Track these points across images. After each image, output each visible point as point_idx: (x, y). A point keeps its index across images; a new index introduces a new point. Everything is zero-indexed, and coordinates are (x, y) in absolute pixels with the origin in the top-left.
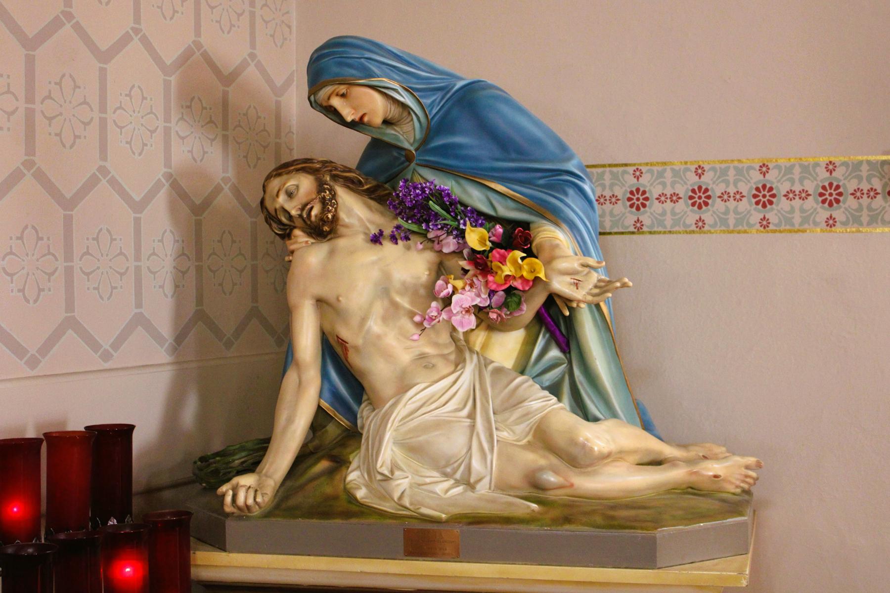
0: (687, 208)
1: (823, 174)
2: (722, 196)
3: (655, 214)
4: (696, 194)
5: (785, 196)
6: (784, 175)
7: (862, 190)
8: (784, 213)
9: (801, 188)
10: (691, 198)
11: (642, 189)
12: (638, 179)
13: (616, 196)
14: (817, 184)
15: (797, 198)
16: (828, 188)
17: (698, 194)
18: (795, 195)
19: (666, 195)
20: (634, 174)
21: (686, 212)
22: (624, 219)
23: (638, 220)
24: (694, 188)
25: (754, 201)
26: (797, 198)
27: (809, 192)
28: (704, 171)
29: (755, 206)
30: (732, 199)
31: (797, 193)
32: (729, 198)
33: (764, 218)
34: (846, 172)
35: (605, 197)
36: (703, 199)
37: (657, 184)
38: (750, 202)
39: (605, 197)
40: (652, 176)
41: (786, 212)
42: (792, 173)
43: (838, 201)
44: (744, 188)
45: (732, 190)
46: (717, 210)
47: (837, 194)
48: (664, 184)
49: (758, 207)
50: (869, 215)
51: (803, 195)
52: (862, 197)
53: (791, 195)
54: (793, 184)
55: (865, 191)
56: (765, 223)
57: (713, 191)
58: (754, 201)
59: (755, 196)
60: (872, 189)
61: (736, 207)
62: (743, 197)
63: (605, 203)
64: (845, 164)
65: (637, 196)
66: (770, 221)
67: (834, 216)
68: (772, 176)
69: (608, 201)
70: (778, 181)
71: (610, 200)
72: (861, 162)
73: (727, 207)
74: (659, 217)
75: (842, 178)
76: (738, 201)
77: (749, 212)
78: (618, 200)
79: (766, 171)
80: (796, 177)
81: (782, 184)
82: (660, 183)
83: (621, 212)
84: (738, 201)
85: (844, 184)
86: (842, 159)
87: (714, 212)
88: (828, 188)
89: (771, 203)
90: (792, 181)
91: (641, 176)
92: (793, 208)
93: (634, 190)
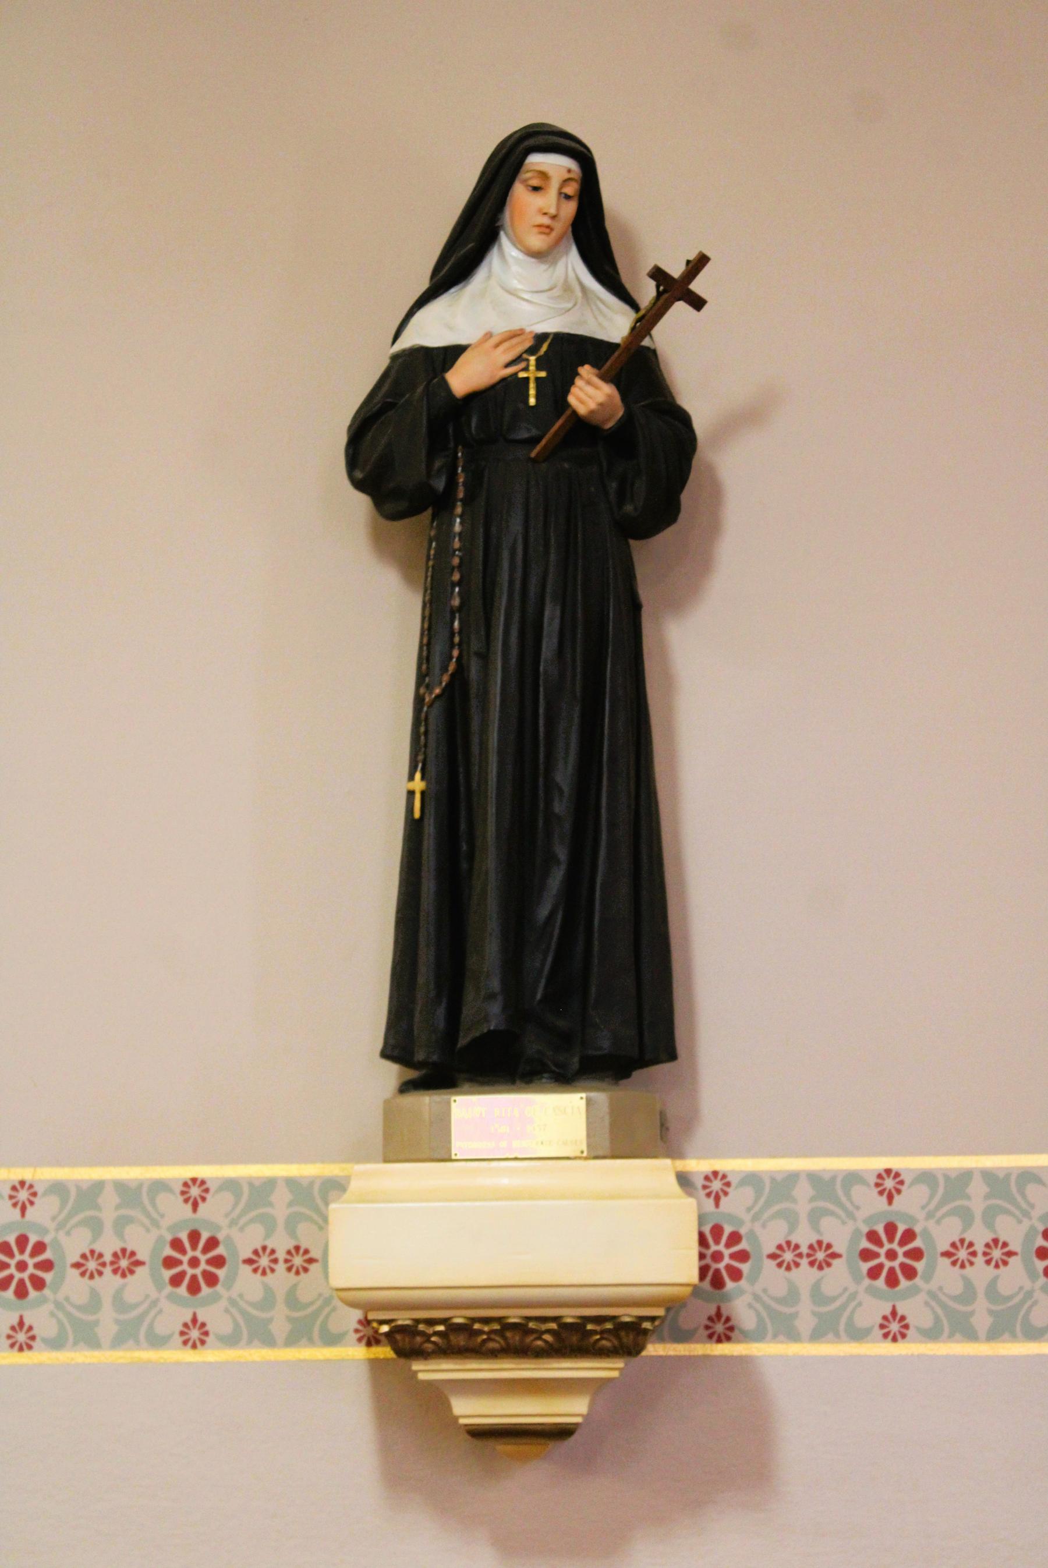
0: (1033, 1282)
3: (242, 1304)
9: (117, 1246)
11: (33, 1239)
13: (306, 1252)
15: (804, 1262)
16: (883, 1237)
18: (104, 1265)
20: (11, 1197)
23: (21, 1323)
26: (108, 1271)
35: (273, 1252)
36: (888, 1264)
39: (797, 1247)
42: (97, 1207)
45: (108, 1246)
47: (209, 1262)
50: (991, 1312)
52: (972, 1263)
63: (273, 1270)
65: (190, 1254)
66: (34, 1332)
69: (980, 1252)
71: (112, 1263)
74: (254, 1312)
76: (297, 1273)
78: (1010, 1254)
79: (723, 1190)
80: (978, 1206)
82: (85, 1222)
88: (883, 1237)
89: (39, 1284)
91: (32, 1203)
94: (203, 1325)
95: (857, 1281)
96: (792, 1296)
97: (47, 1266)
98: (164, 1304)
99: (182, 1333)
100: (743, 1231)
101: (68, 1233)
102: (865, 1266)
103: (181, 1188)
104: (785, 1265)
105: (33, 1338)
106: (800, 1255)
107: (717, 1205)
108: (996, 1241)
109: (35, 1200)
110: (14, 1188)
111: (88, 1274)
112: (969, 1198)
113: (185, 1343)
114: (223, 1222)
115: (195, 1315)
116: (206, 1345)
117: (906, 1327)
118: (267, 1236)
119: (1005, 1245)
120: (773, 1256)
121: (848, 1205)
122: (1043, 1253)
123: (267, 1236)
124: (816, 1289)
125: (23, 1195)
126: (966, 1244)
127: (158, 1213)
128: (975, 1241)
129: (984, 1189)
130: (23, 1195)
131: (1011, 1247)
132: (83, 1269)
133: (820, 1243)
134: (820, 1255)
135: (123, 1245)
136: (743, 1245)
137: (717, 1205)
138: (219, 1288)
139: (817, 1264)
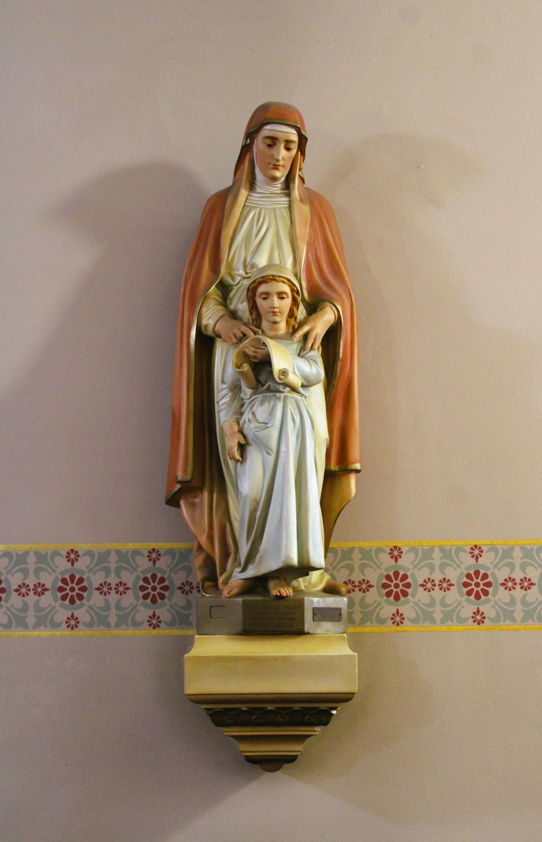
1: (63, 565)
2: (101, 587)
3: (12, 609)
4: (67, 585)
5: (16, 590)
7: (109, 584)
8: (423, 606)
9: (522, 576)
10: (466, 585)
19: (433, 581)
21: (89, 606)
22: (54, 614)
27: (533, 581)
28: (78, 556)
30: (437, 588)
32: (110, 591)
33: (154, 615)
34: (9, 565)
40: (417, 556)
41: (17, 610)
42: (26, 563)
43: (405, 594)
44: (47, 579)
48: (512, 566)
51: (526, 584)
53: (510, 584)
54: (512, 571)
55: (113, 586)
56: (479, 617)
59: (142, 588)
60: (121, 583)
61: (443, 598)
62: (127, 589)
64: (90, 553)
67: (76, 615)
68: (486, 560)
69: (195, 587)
70: (495, 566)
71: (520, 584)
73: (512, 597)
75: (87, 570)
77: (460, 603)
83: (537, 599)
84: (121, 594)
90: (26, 573)
92: (25, 606)
94: (402, 615)
97: (166, 588)
98: (465, 604)
101: (499, 570)
102: (465, 590)
104: (508, 588)
105: (484, 618)
106: (355, 586)
107: (477, 561)
111: (22, 595)
112: (433, 559)
113: (68, 627)
115: (398, 610)
117: (403, 619)
118: (431, 573)
119: (125, 584)
122: (3, 590)
123: (431, 573)
124: (36, 605)
126: (431, 581)
127: (55, 566)
128: (435, 579)
129: (116, 558)
130: (154, 555)
132: (19, 592)
133: (39, 584)
135: (39, 581)
137: (477, 561)
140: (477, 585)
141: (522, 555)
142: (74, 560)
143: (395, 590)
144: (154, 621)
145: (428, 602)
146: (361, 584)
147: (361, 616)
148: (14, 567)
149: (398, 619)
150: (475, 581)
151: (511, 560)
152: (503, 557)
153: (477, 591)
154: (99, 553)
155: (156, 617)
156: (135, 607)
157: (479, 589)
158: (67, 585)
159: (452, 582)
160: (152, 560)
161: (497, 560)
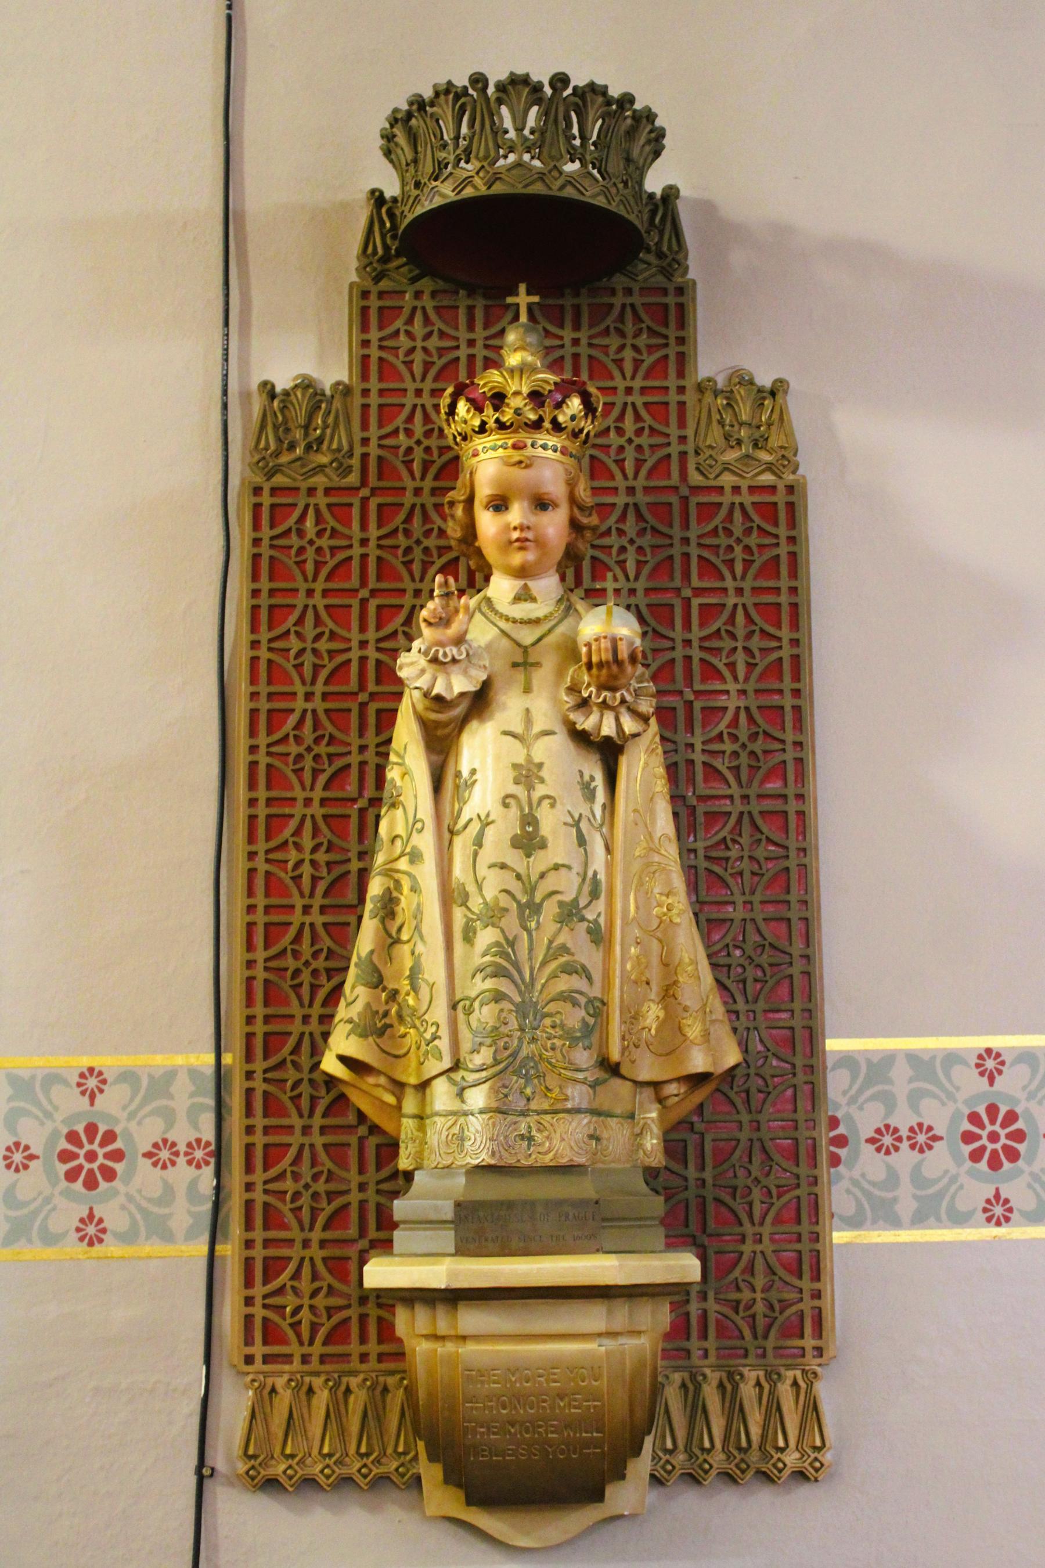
6: (936, 1082)
12: (92, 1098)
14: (957, 1110)
17: (989, 1128)
24: (75, 1128)
25: (62, 1168)
29: (64, 1184)
31: (182, 1148)
33: (91, 1216)
34: (1031, 1080)
36: (990, 1146)
37: (151, 1113)
38: (50, 1173)
46: (140, 1191)
49: (977, 1165)
50: (915, 1197)
51: (164, 1155)
53: (164, 1155)
56: (91, 1230)
57: (129, 1136)
58: (62, 1168)
64: (128, 1076)
71: (909, 1138)
72: (171, 1074)
81: (861, 1108)
82: (156, 1112)
85: (126, 1130)
86: (127, 1061)
87: (130, 1198)
89: (109, 1175)
93: (80, 1128)
95: (959, 1163)
96: (892, 1179)
98: (60, 1201)
99: (985, 1210)
100: (118, 1130)
102: (967, 1149)
103: (76, 1079)
105: (104, 1231)
108: (17, 1145)
109: (1004, 1069)
110: (82, 1075)
114: (1021, 1095)
116: (1010, 1223)
117: (1010, 1210)
120: (148, 1155)
121: (947, 1085)
125: (92, 1083)
130: (92, 1083)
131: (33, 1151)
134: (921, 1138)
136: (118, 1144)
138: (1021, 1163)
139: (918, 1146)
140: (91, 1156)
141: (910, 1073)
142: (96, 1090)
143: (990, 1146)
144: (91, 1230)
145: (157, 1194)
146: (915, 1132)
147: (915, 1205)
148: (38, 1104)
149: (998, 1210)
150: (87, 1147)
151: (887, 1087)
152: (869, 1082)
153: (91, 1172)
154: (151, 1077)
155: (96, 1220)
156: (48, 1200)
157: (95, 1166)
158: (982, 1127)
159: (938, 1131)
160: (88, 1093)
161: (856, 1087)
